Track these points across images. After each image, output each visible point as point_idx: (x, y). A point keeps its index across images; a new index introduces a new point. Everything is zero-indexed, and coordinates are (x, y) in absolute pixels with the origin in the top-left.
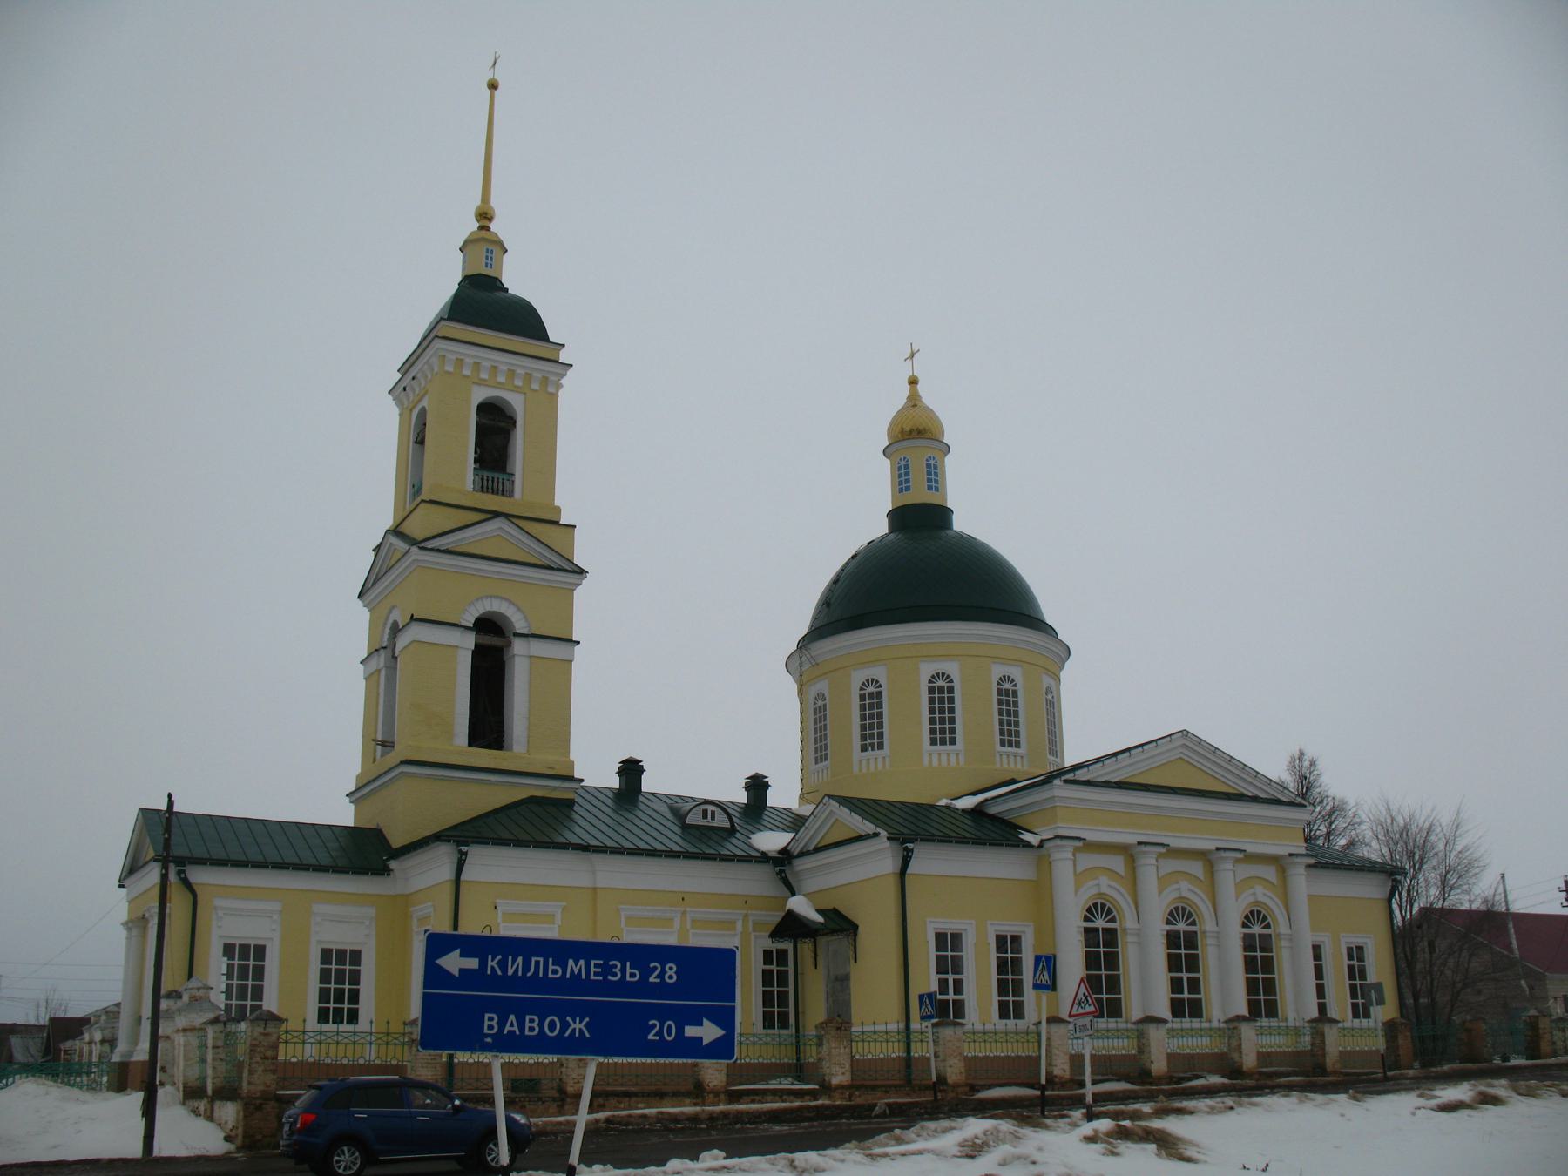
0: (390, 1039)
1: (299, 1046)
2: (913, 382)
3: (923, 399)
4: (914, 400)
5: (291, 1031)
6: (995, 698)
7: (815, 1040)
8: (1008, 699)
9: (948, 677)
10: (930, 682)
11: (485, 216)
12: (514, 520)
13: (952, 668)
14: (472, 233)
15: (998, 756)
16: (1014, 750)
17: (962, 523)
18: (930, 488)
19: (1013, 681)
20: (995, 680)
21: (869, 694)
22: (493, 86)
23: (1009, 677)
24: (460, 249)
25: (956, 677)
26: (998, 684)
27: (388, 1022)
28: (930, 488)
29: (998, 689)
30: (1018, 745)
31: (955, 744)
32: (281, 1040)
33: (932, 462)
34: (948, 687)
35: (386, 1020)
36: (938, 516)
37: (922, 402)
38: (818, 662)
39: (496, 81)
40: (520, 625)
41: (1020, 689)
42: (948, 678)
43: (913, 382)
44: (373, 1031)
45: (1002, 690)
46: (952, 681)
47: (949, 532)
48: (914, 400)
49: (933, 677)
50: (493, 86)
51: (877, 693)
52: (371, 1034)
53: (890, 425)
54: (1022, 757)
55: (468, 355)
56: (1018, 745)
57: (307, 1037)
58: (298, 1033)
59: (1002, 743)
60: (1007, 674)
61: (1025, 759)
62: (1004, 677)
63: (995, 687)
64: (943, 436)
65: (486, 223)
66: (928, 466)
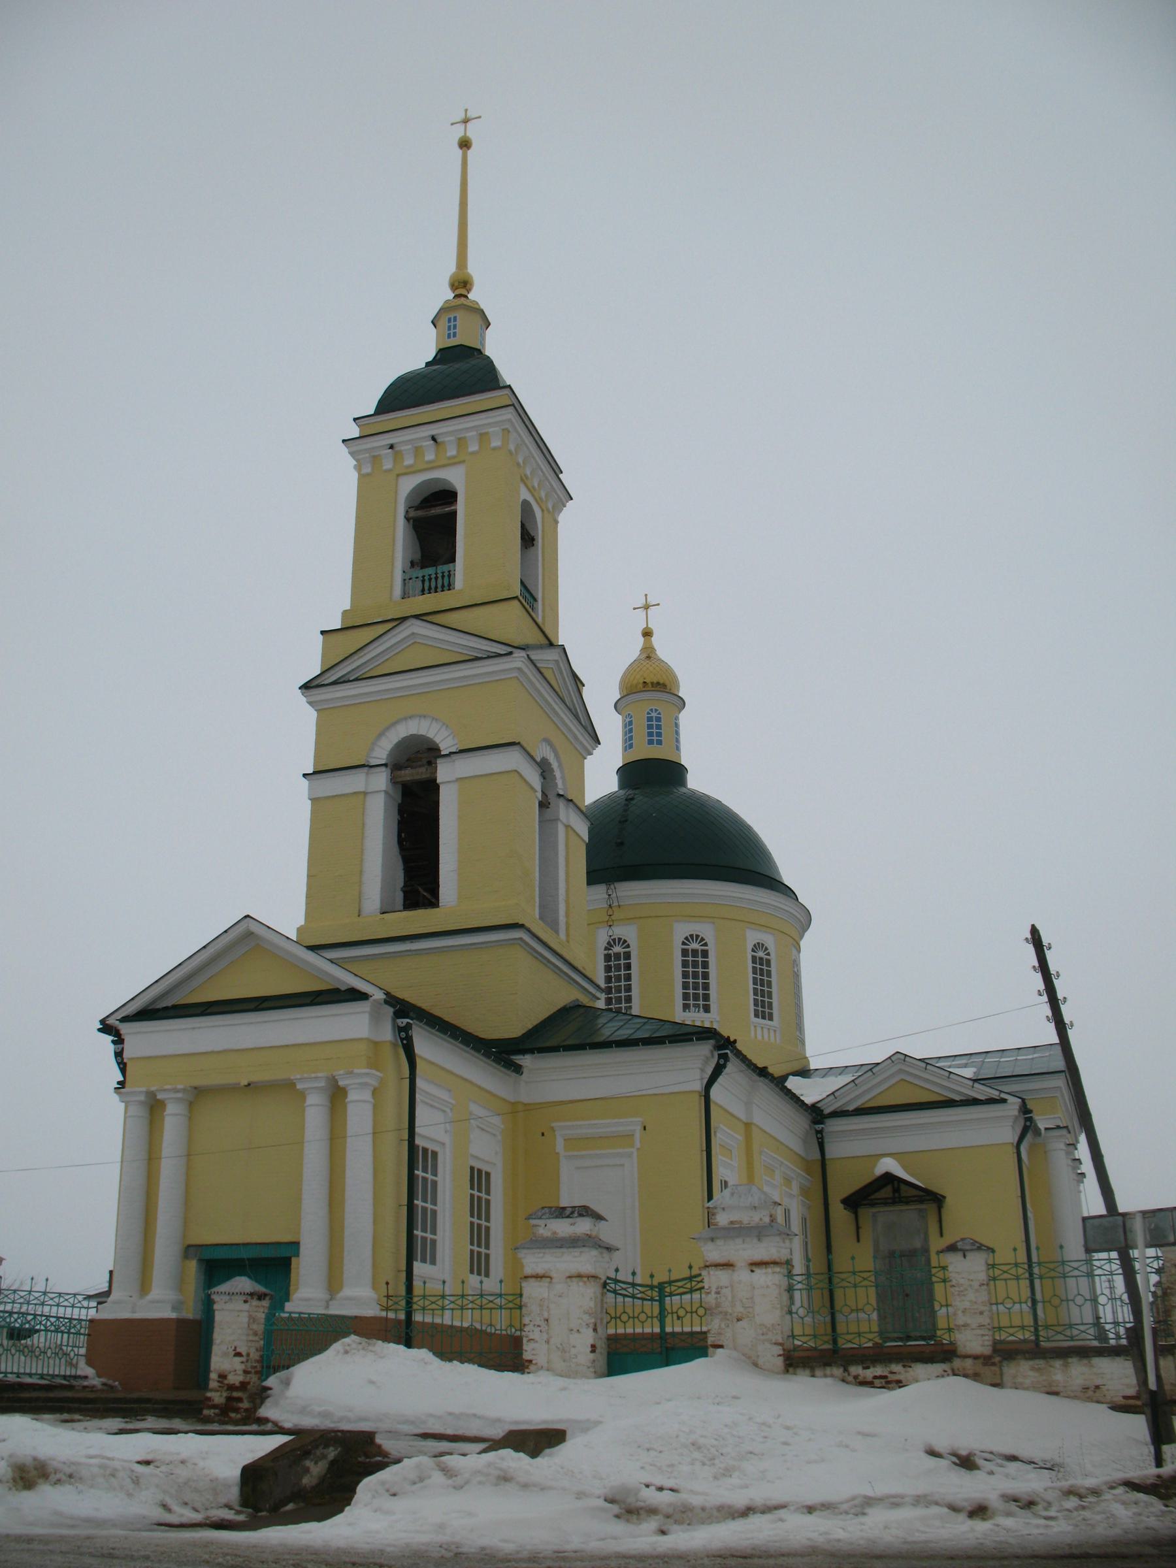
0: (427, 1303)
1: (477, 1313)
2: (647, 634)
3: (658, 652)
4: (648, 653)
5: (1044, 1263)
6: (750, 965)
7: (1091, 1331)
8: (761, 966)
9: (703, 939)
10: (684, 943)
11: (461, 284)
12: (424, 618)
13: (706, 930)
14: (447, 302)
15: (752, 1028)
16: (767, 1022)
17: (696, 782)
18: (651, 742)
19: (766, 949)
20: (750, 947)
21: (692, 950)
22: (465, 144)
23: (763, 945)
24: (433, 322)
25: (710, 939)
26: (753, 951)
27: (47, 1280)
28: (651, 742)
29: (753, 956)
30: (771, 1019)
31: (709, 1012)
32: (657, 1290)
33: (654, 715)
34: (702, 951)
35: (385, 1282)
36: (673, 772)
37: (656, 654)
38: (621, 904)
39: (468, 137)
40: (446, 746)
41: (773, 958)
42: (624, 943)
43: (647, 634)
44: (447, 1293)
45: (688, 950)
46: (706, 945)
47: (683, 790)
48: (648, 653)
49: (686, 938)
50: (465, 144)
51: (624, 953)
52: (443, 1297)
53: (625, 673)
54: (775, 1031)
55: (468, 429)
56: (771, 1019)
57: (1068, 1269)
58: (1009, 1267)
59: (756, 1016)
60: (761, 942)
61: (778, 1034)
62: (758, 943)
63: (749, 954)
64: (678, 691)
65: (463, 292)
66: (650, 719)
